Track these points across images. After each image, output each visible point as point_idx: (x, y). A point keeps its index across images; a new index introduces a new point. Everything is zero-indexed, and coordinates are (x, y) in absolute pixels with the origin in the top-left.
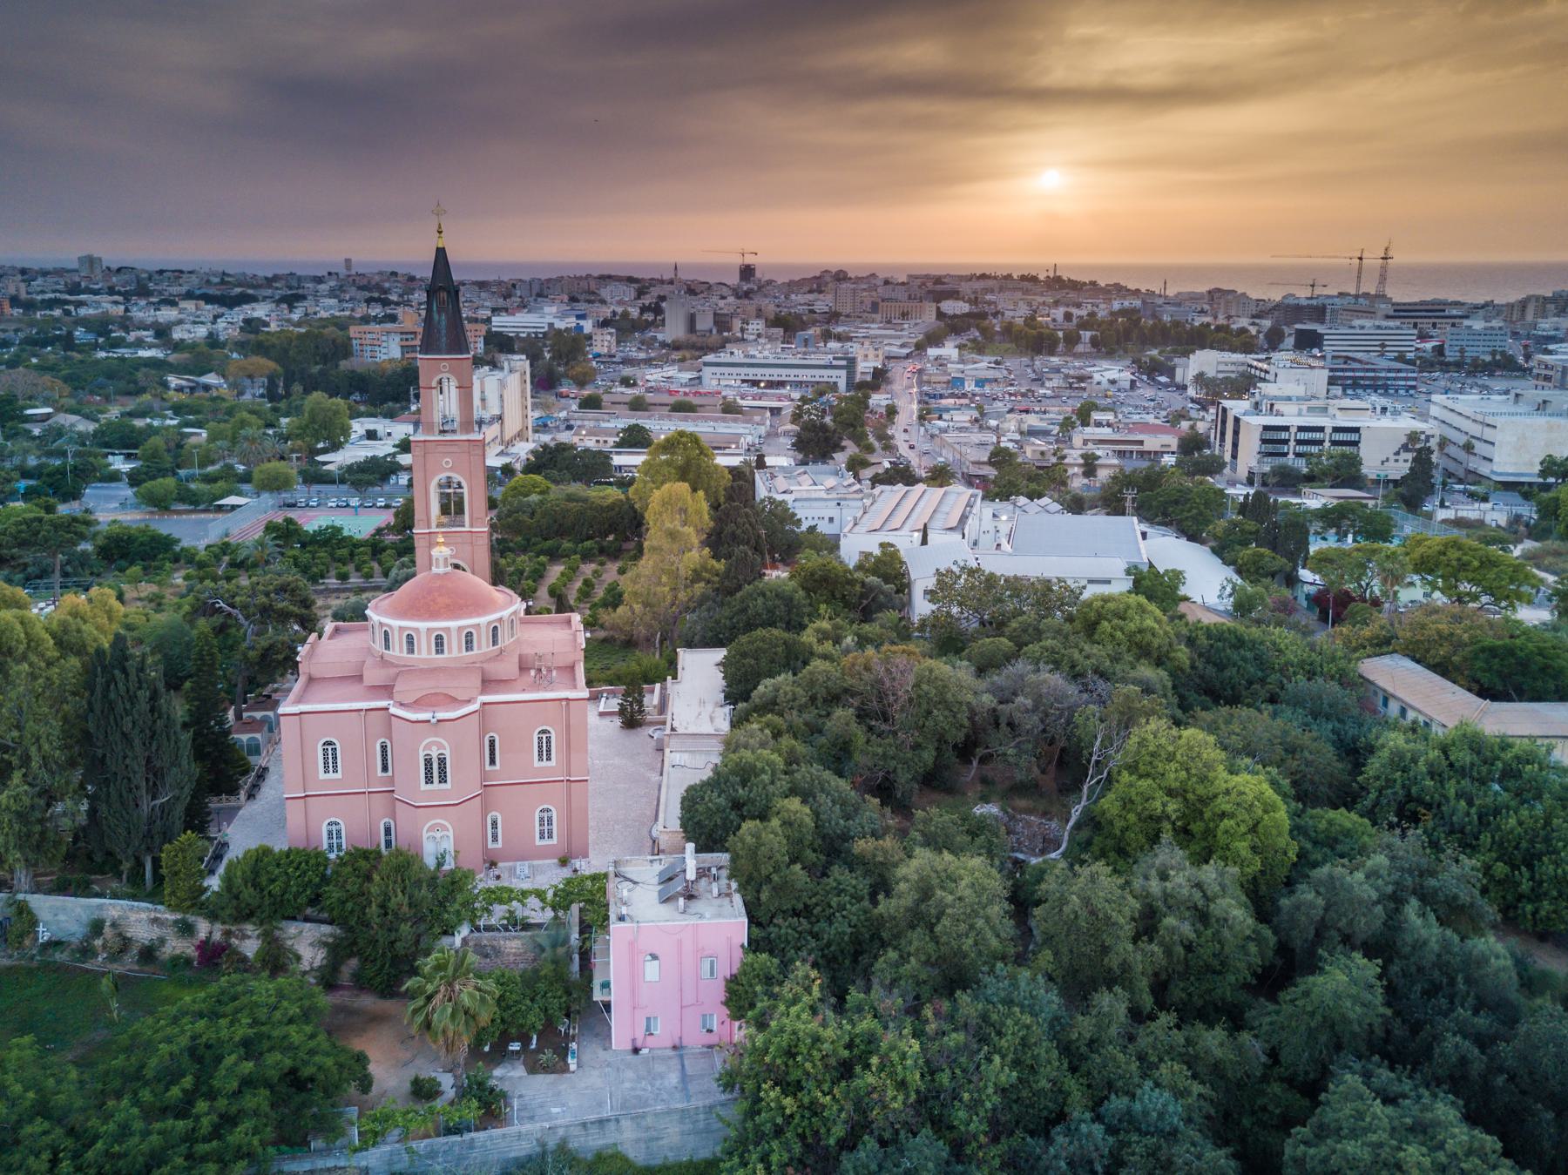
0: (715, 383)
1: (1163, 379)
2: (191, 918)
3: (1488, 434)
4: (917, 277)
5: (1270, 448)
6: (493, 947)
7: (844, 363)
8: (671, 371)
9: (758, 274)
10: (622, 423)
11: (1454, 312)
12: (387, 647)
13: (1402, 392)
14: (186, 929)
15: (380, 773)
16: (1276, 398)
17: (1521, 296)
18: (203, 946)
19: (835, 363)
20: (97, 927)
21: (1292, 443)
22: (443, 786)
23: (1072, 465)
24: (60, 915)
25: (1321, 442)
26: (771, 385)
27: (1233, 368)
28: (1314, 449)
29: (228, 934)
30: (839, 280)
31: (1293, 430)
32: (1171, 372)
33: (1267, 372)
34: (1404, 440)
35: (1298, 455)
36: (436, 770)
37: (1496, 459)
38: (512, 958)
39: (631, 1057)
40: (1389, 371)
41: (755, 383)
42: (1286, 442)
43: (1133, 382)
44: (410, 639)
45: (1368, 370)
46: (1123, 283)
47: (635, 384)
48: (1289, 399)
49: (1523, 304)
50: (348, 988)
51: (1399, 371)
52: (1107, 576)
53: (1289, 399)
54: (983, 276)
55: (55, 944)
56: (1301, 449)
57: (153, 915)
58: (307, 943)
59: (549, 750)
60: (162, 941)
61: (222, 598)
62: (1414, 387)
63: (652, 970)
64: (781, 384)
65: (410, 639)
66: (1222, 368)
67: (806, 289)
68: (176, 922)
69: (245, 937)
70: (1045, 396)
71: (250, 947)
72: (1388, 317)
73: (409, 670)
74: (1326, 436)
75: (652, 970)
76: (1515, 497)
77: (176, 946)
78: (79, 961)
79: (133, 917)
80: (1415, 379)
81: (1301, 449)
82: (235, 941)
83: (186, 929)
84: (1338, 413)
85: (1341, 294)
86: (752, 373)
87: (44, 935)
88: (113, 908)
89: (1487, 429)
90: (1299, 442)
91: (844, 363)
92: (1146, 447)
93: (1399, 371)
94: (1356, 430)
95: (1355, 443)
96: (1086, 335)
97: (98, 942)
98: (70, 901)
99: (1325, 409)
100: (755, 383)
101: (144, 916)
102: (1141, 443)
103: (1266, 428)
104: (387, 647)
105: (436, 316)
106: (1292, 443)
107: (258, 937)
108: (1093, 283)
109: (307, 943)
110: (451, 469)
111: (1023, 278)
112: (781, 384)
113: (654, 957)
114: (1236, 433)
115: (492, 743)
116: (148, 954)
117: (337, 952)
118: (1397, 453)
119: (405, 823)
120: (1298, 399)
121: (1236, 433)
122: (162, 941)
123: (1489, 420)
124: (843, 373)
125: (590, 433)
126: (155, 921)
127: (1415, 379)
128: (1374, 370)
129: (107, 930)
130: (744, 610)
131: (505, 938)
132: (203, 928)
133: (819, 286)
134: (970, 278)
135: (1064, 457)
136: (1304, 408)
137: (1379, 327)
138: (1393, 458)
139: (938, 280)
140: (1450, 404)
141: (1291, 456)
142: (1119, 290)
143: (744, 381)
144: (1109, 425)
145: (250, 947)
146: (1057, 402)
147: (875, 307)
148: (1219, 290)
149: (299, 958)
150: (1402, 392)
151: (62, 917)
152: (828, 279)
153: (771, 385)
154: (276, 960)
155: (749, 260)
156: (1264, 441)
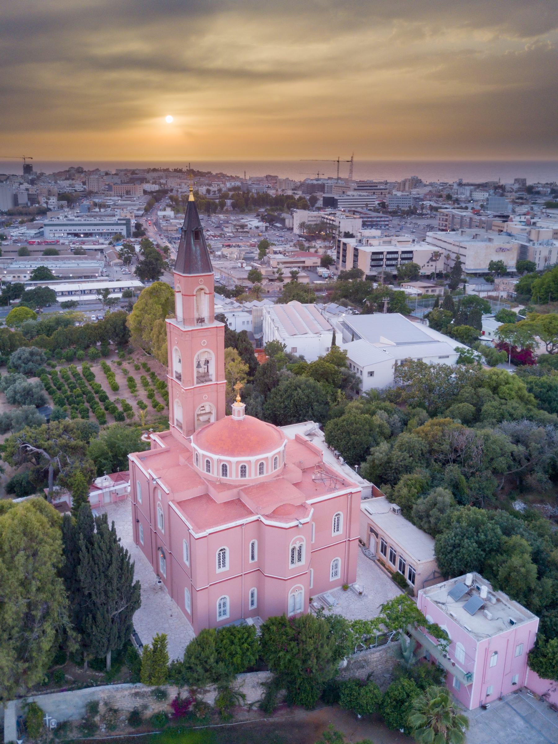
0: (52, 235)
1: (278, 225)
2: (162, 688)
3: (462, 251)
4: (121, 171)
5: (374, 263)
6: (365, 661)
7: (124, 222)
8: (23, 229)
9: (34, 170)
10: (36, 265)
11: (382, 187)
12: (208, 471)
13: (383, 227)
14: (161, 695)
15: (251, 561)
16: (368, 237)
17: (403, 179)
18: (176, 704)
19: (119, 222)
20: (93, 707)
21: (385, 260)
22: (300, 564)
23: (286, 277)
24: (61, 706)
25: (396, 259)
26: (86, 235)
27: (315, 219)
28: (394, 262)
29: (193, 692)
30: (79, 172)
31: (385, 254)
32: (283, 221)
33: (333, 221)
34: (431, 256)
35: (387, 266)
36: (296, 554)
37: (467, 263)
38: (375, 664)
39: (483, 712)
40: (377, 217)
41: (77, 235)
42: (382, 260)
43: (266, 227)
44: (224, 467)
45: (368, 218)
46: (224, 173)
47: (6, 239)
48: (374, 237)
49: (404, 183)
50: (281, 708)
51: (381, 217)
52: (448, 354)
53: (374, 237)
54: (154, 170)
55: (62, 726)
56: (389, 262)
57: (133, 691)
58: (251, 687)
59: (338, 525)
60: (145, 707)
61: (29, 442)
62: (388, 225)
63: (493, 661)
64: (91, 235)
65: (224, 467)
66: (310, 219)
67: (64, 178)
68: (152, 692)
69: (206, 691)
70: (230, 236)
71: (210, 697)
72: (355, 190)
73: (247, 490)
74: (399, 256)
75: (493, 661)
76: (482, 280)
77: (155, 707)
78: (89, 735)
79: (118, 695)
80: (388, 221)
81: (389, 262)
82: (199, 696)
83: (161, 695)
84: (397, 244)
85: (329, 178)
86: (77, 229)
87: (52, 722)
88: (100, 693)
89: (461, 249)
90: (388, 259)
91: (124, 222)
92: (307, 264)
93: (381, 217)
94: (411, 252)
95: (411, 259)
96: (229, 202)
97: (97, 719)
98: (69, 695)
99: (390, 242)
100: (77, 235)
101: (126, 693)
102: (304, 262)
103: (374, 253)
104: (208, 471)
105: (194, 248)
106: (385, 260)
107: (215, 689)
108: (209, 173)
109: (251, 687)
110: (206, 347)
111: (176, 170)
112: (91, 235)
113: (496, 653)
114: (356, 256)
115: (253, 558)
116: (135, 717)
117: (271, 687)
118: (428, 262)
119: (271, 591)
120: (379, 237)
121: (356, 256)
122: (145, 707)
123: (462, 244)
124: (124, 227)
125: (10, 272)
126: (136, 694)
127: (388, 221)
128: (371, 217)
129: (102, 708)
130: (291, 396)
131: (371, 653)
132: (173, 692)
133: (70, 176)
134: (148, 171)
135: (282, 274)
136: (381, 241)
137: (360, 195)
138: (426, 264)
139: (133, 172)
140: (436, 236)
141: (384, 266)
142: (221, 177)
143: (68, 234)
144: (280, 253)
145: (210, 697)
146: (236, 239)
147: (110, 188)
148: (270, 176)
149: (244, 696)
150: (383, 227)
151: (63, 707)
152: (73, 171)
153: (86, 235)
154: (229, 699)
155: (28, 161)
156: (373, 260)
